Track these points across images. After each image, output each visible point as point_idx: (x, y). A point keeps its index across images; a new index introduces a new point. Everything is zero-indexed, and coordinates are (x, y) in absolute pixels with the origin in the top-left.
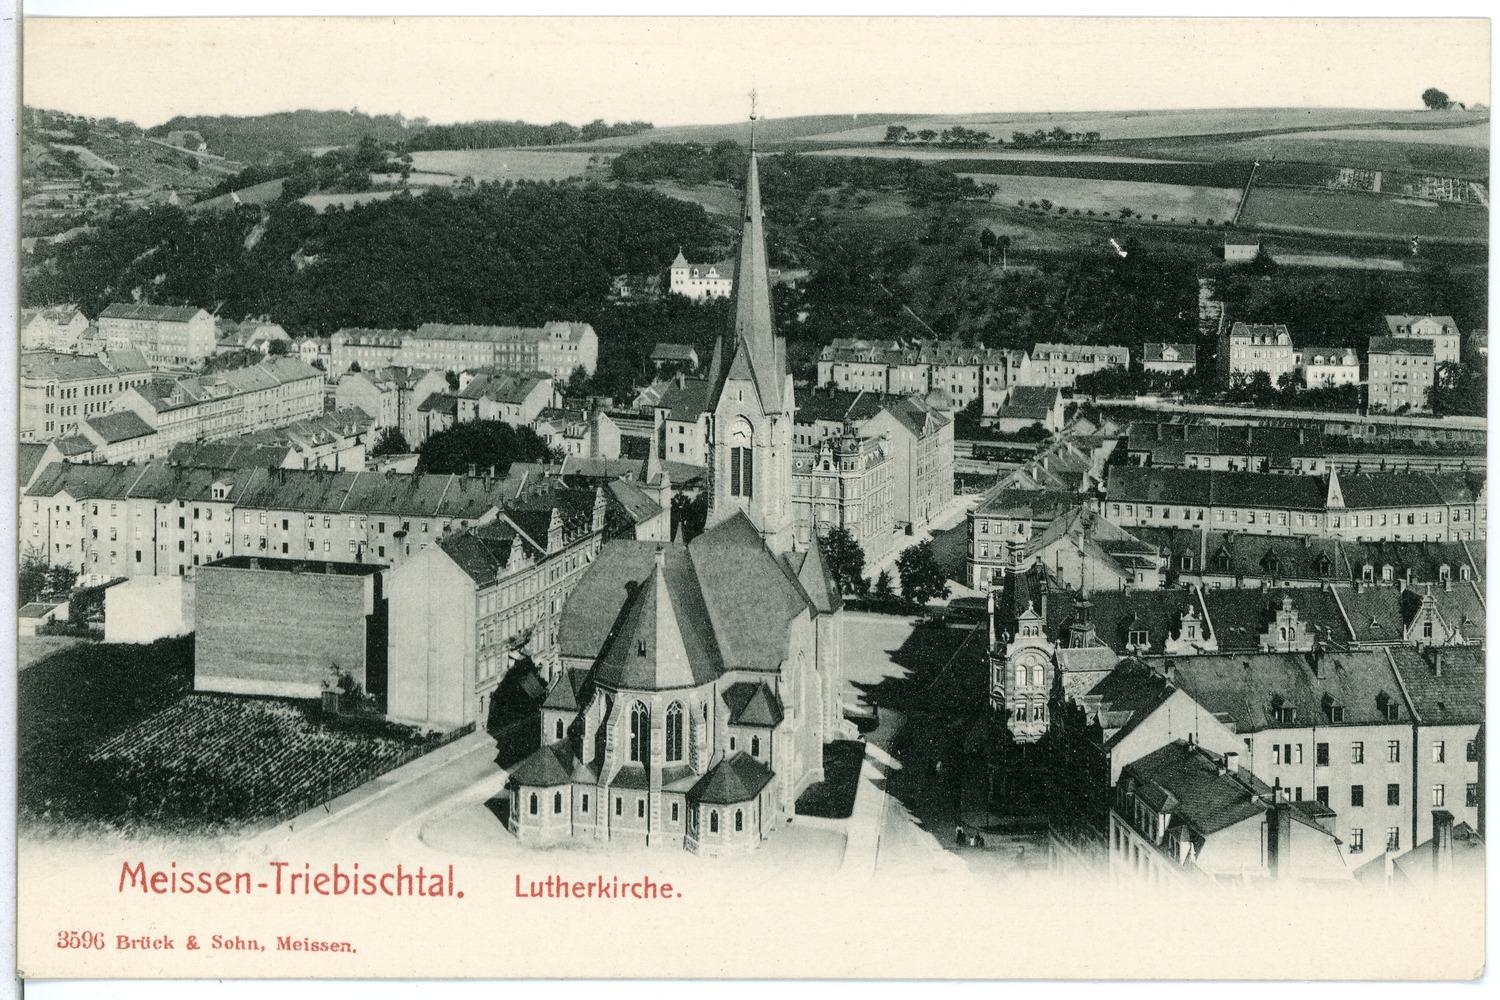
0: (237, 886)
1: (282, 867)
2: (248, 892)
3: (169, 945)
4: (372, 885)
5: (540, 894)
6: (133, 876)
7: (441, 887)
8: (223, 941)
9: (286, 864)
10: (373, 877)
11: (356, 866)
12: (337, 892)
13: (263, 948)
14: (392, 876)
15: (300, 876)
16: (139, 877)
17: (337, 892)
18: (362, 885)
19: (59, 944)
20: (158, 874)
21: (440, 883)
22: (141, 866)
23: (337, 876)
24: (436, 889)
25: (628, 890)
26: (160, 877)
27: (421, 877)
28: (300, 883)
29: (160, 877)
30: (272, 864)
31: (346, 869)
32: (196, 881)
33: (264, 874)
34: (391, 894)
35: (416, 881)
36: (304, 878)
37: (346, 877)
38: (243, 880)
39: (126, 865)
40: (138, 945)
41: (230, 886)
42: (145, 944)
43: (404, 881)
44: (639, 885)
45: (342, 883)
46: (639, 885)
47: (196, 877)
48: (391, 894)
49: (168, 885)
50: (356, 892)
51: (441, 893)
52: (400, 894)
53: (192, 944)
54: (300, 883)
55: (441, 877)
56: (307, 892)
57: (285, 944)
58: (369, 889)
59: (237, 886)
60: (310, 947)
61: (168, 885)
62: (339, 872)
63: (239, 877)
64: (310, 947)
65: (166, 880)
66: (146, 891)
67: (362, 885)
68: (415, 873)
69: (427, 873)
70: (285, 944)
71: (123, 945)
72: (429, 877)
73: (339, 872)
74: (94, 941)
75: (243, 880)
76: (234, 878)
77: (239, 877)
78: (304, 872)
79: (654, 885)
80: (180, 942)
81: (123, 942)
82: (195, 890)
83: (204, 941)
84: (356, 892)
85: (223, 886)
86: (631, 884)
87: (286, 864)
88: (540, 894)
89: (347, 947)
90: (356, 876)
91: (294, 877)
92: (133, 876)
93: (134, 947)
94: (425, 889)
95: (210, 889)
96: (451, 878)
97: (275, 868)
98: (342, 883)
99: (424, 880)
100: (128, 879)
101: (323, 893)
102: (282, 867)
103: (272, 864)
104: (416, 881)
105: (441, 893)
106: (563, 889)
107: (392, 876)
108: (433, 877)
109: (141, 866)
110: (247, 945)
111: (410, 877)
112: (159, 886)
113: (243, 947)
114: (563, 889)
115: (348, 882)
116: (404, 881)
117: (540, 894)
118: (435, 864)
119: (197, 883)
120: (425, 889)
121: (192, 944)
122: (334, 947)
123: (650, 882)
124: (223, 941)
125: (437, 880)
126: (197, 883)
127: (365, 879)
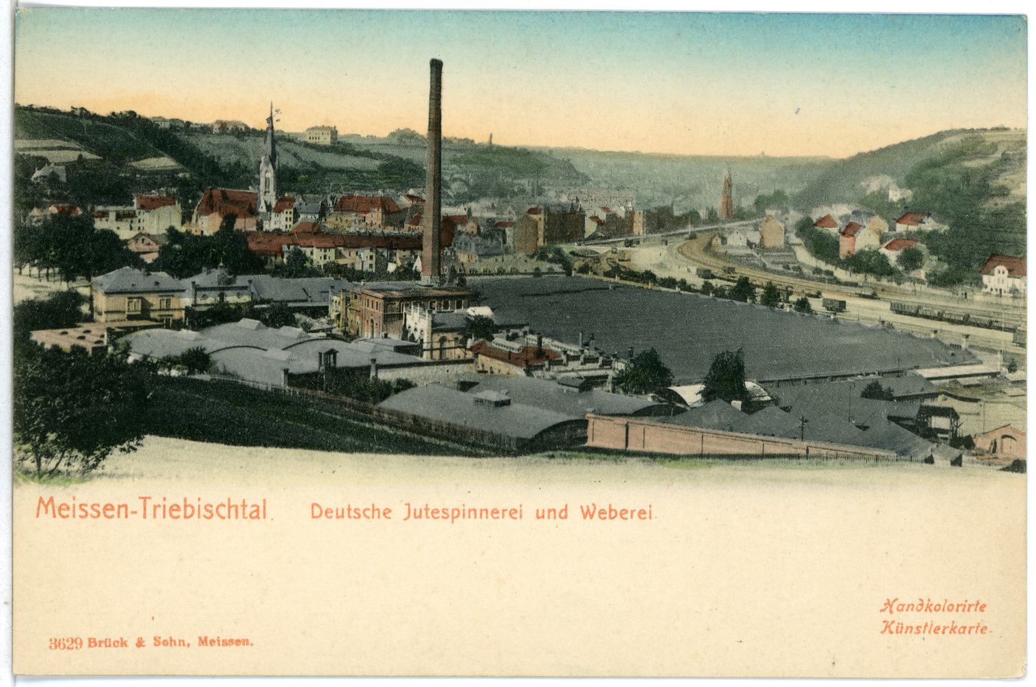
0: (119, 513)
1: (147, 500)
2: (237, 518)
3: (123, 643)
4: (210, 512)
5: (420, 516)
6: (46, 507)
7: (258, 513)
8: (161, 640)
9: (150, 498)
10: (98, 505)
11: (199, 499)
12: (186, 517)
13: (189, 645)
14: (224, 506)
15: (160, 506)
16: (50, 507)
17: (186, 517)
18: (203, 512)
19: (50, 647)
20: (62, 505)
21: (257, 511)
22: (51, 500)
23: (186, 506)
24: (254, 514)
25: (507, 514)
26: (175, 508)
27: (244, 506)
28: (160, 511)
29: (109, 507)
30: (140, 498)
31: (192, 501)
32: (88, 509)
33: (136, 505)
34: (223, 518)
35: (240, 511)
36: (162, 508)
37: (192, 507)
38: (123, 510)
39: (41, 500)
40: (103, 645)
41: (628, 516)
42: (108, 644)
43: (233, 509)
44: (369, 509)
45: (189, 511)
46: (369, 509)
47: (89, 506)
48: (223, 518)
49: (70, 513)
50: (199, 517)
51: (258, 517)
52: (229, 517)
53: (140, 643)
54: (160, 511)
55: (258, 507)
56: (264, 500)
57: (203, 641)
58: (208, 515)
59: (119, 513)
60: (221, 643)
61: (70, 513)
62: (188, 503)
63: (120, 507)
64: (221, 643)
65: (68, 508)
66: (55, 516)
67: (203, 512)
68: (239, 503)
69: (249, 503)
70: (203, 641)
71: (93, 644)
72: (249, 506)
73: (188, 503)
74: (75, 642)
75: (123, 510)
76: (116, 508)
77: (120, 507)
78: (161, 503)
79: (378, 509)
80: (132, 643)
81: (93, 642)
82: (89, 516)
83: (149, 642)
84: (199, 517)
85: (624, 516)
86: (509, 510)
87: (150, 498)
88: (420, 516)
89: (245, 642)
90: (199, 506)
91: (155, 507)
92: (46, 507)
93: (100, 646)
94: (247, 515)
95: (212, 515)
96: (264, 509)
97: (142, 501)
98: (189, 511)
99: (246, 508)
100: (42, 507)
101: (624, 518)
102: (147, 500)
103: (140, 498)
104: (240, 511)
105: (258, 517)
106: (376, 512)
107: (224, 506)
108: (252, 506)
109: (51, 500)
110: (178, 643)
111: (236, 507)
112: (63, 513)
113: (175, 645)
114: (376, 512)
115: (193, 511)
116: (233, 509)
117: (343, 516)
118: (254, 498)
119: (90, 511)
120: (247, 515)
121: (140, 643)
122: (238, 642)
123: (376, 507)
124: (161, 640)
125: (255, 508)
126: (90, 511)
127: (205, 508)
